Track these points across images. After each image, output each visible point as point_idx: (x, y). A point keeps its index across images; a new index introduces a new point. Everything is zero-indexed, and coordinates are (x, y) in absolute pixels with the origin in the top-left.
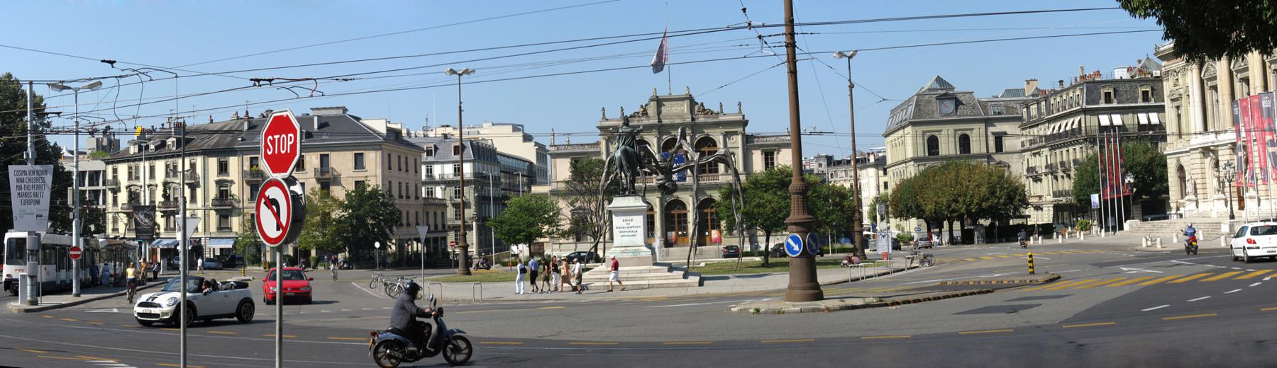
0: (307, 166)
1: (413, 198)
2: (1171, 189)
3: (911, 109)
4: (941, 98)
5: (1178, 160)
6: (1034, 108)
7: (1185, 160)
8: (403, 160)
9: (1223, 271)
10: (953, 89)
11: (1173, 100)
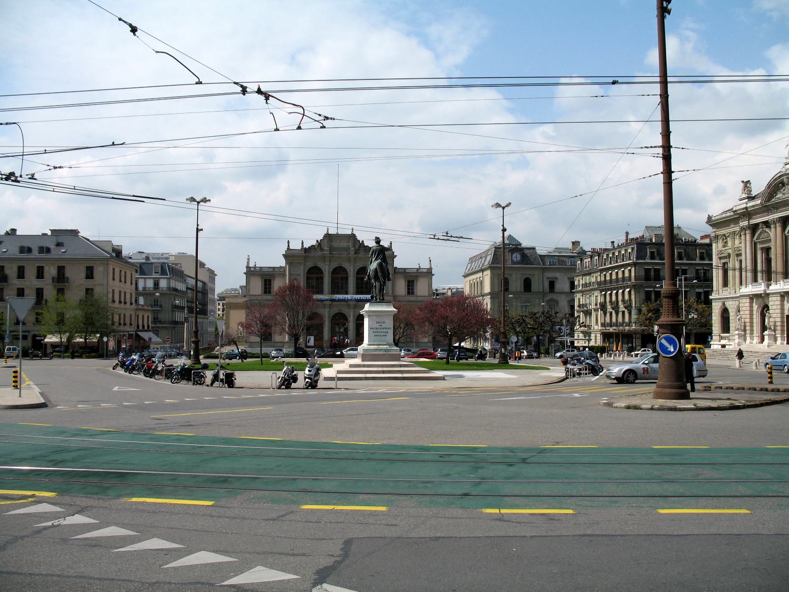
0: (46, 275)
1: (128, 304)
2: (714, 325)
3: (489, 258)
4: (513, 251)
5: (724, 304)
6: (587, 261)
7: (731, 306)
8: (123, 273)
9: (611, 391)
10: (520, 245)
11: (720, 258)
